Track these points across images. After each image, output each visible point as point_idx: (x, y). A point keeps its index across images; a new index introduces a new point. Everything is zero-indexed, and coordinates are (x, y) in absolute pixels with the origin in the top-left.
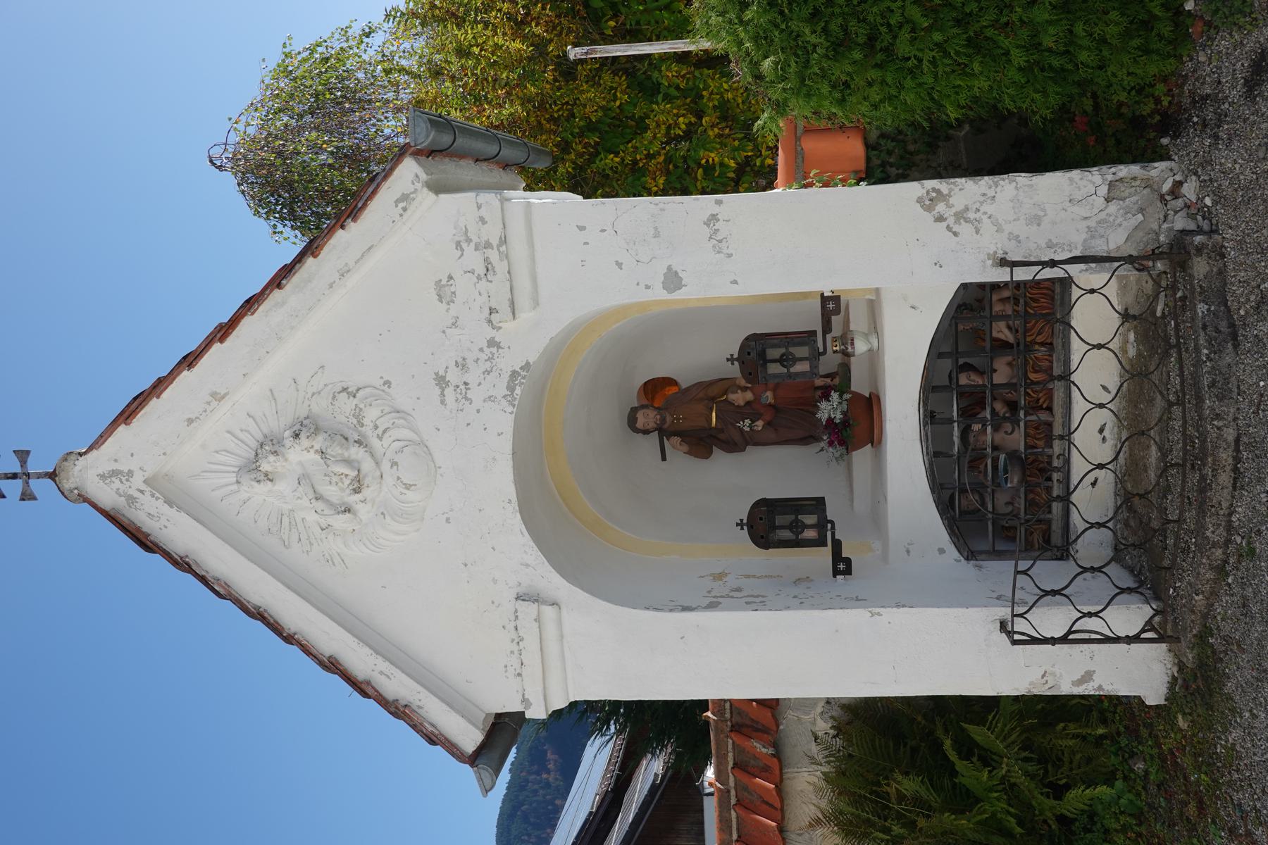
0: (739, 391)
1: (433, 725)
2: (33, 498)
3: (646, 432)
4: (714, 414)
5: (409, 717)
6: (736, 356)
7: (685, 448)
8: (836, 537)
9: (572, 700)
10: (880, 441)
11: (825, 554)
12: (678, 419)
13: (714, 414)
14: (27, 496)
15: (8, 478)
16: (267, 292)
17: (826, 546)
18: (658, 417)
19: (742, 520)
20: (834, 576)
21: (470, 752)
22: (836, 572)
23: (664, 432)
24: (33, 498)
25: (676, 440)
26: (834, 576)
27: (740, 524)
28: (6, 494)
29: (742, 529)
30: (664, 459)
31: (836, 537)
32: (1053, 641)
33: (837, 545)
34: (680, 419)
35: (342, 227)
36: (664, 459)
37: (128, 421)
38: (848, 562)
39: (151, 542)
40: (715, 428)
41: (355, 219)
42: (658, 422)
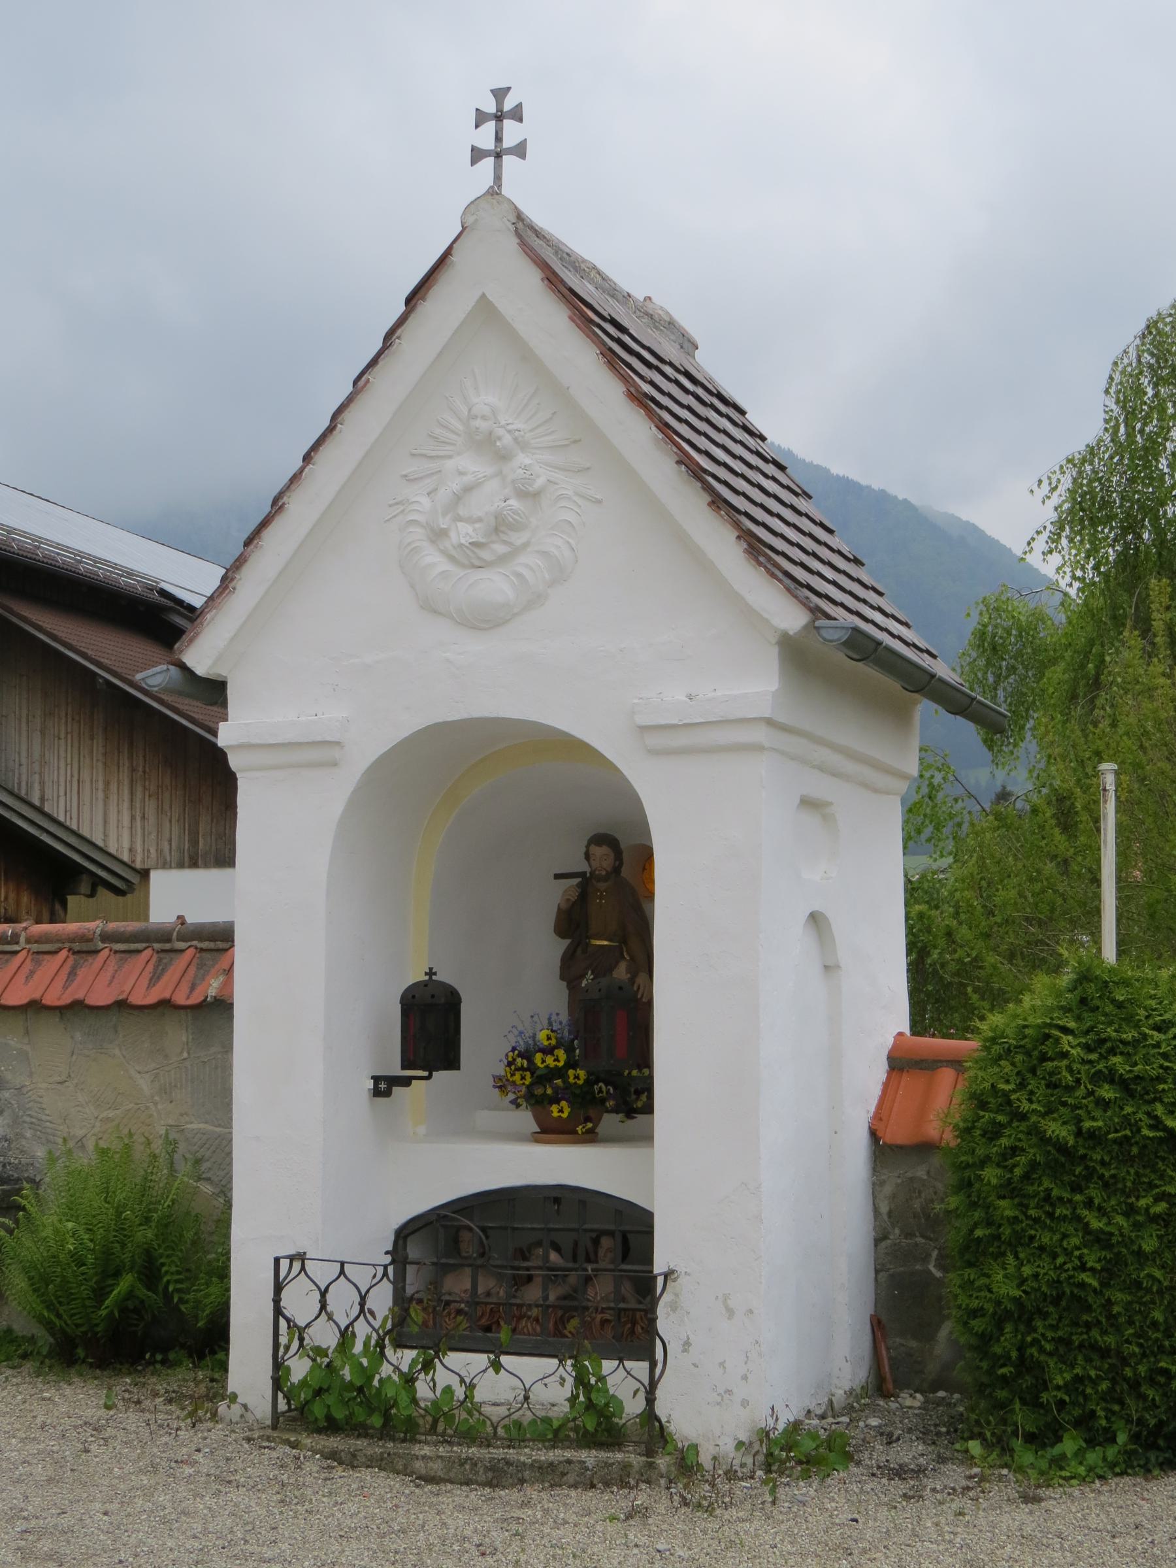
0: (629, 975)
1: (213, 619)
2: (474, 162)
3: (587, 856)
4: (606, 943)
5: (221, 593)
6: (434, 978)
7: (564, 906)
8: (413, 1081)
9: (238, 776)
10: (537, 1141)
11: (395, 1069)
12: (601, 898)
13: (606, 943)
14: (477, 155)
15: (497, 133)
16: (675, 450)
17: (404, 1067)
18: (604, 873)
19: (435, 974)
20: (373, 1077)
21: (184, 660)
22: (376, 1079)
23: (586, 882)
24: (474, 162)
25: (574, 895)
26: (373, 1077)
27: (431, 973)
28: (479, 129)
29: (426, 974)
30: (558, 876)
31: (413, 1081)
32: (277, 1301)
33: (406, 1082)
34: (601, 900)
35: (739, 537)
36: (558, 876)
37: (546, 282)
38: (387, 1093)
39: (416, 304)
40: (588, 945)
41: (746, 551)
42: (597, 872)
